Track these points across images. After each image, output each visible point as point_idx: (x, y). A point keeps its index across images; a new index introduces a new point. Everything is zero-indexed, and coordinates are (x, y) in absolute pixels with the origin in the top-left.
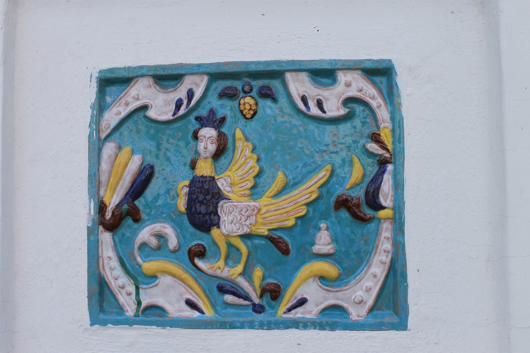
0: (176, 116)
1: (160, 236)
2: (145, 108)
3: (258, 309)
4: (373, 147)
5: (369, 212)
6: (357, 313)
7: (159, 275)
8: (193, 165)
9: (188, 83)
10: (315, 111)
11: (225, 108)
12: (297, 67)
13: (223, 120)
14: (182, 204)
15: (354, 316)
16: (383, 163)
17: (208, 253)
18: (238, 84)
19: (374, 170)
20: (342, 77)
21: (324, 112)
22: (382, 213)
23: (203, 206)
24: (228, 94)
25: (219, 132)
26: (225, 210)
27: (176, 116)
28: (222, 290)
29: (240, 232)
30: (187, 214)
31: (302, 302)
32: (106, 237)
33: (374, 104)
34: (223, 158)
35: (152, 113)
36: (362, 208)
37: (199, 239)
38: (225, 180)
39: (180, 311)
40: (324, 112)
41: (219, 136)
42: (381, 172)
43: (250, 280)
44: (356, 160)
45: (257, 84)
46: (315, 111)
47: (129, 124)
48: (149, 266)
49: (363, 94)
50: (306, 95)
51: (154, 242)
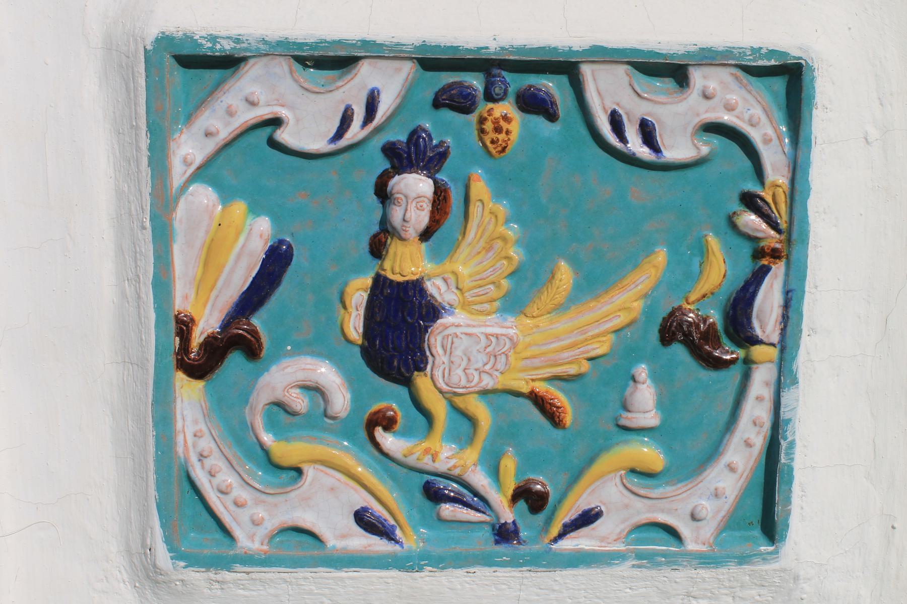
0: (343, 143)
1: (315, 390)
2: (276, 122)
3: (505, 534)
4: (750, 220)
5: (729, 351)
6: (695, 539)
7: (305, 467)
8: (377, 249)
9: (367, 75)
10: (636, 145)
11: (448, 129)
12: (604, 56)
13: (443, 156)
14: (355, 326)
15: (691, 546)
16: (763, 257)
17: (398, 427)
18: (476, 82)
19: (746, 267)
20: (697, 77)
21: (656, 149)
22: (757, 351)
23: (398, 330)
24: (455, 101)
25: (436, 182)
26: (145, 299)
27: (343, 143)
28: (433, 495)
29: (488, 382)
30: (362, 347)
31: (588, 518)
32: (189, 392)
33: (755, 136)
34: (207, 113)
35: (284, 136)
36: (719, 339)
37: (390, 398)
38: (445, 280)
39: (344, 537)
40: (656, 149)
41: (435, 193)
42: (758, 277)
43: (495, 472)
44: (714, 242)
45: (516, 82)
46: (636, 145)
47: (231, 151)
48: (287, 450)
49: (738, 117)
50: (621, 111)
51: (300, 402)
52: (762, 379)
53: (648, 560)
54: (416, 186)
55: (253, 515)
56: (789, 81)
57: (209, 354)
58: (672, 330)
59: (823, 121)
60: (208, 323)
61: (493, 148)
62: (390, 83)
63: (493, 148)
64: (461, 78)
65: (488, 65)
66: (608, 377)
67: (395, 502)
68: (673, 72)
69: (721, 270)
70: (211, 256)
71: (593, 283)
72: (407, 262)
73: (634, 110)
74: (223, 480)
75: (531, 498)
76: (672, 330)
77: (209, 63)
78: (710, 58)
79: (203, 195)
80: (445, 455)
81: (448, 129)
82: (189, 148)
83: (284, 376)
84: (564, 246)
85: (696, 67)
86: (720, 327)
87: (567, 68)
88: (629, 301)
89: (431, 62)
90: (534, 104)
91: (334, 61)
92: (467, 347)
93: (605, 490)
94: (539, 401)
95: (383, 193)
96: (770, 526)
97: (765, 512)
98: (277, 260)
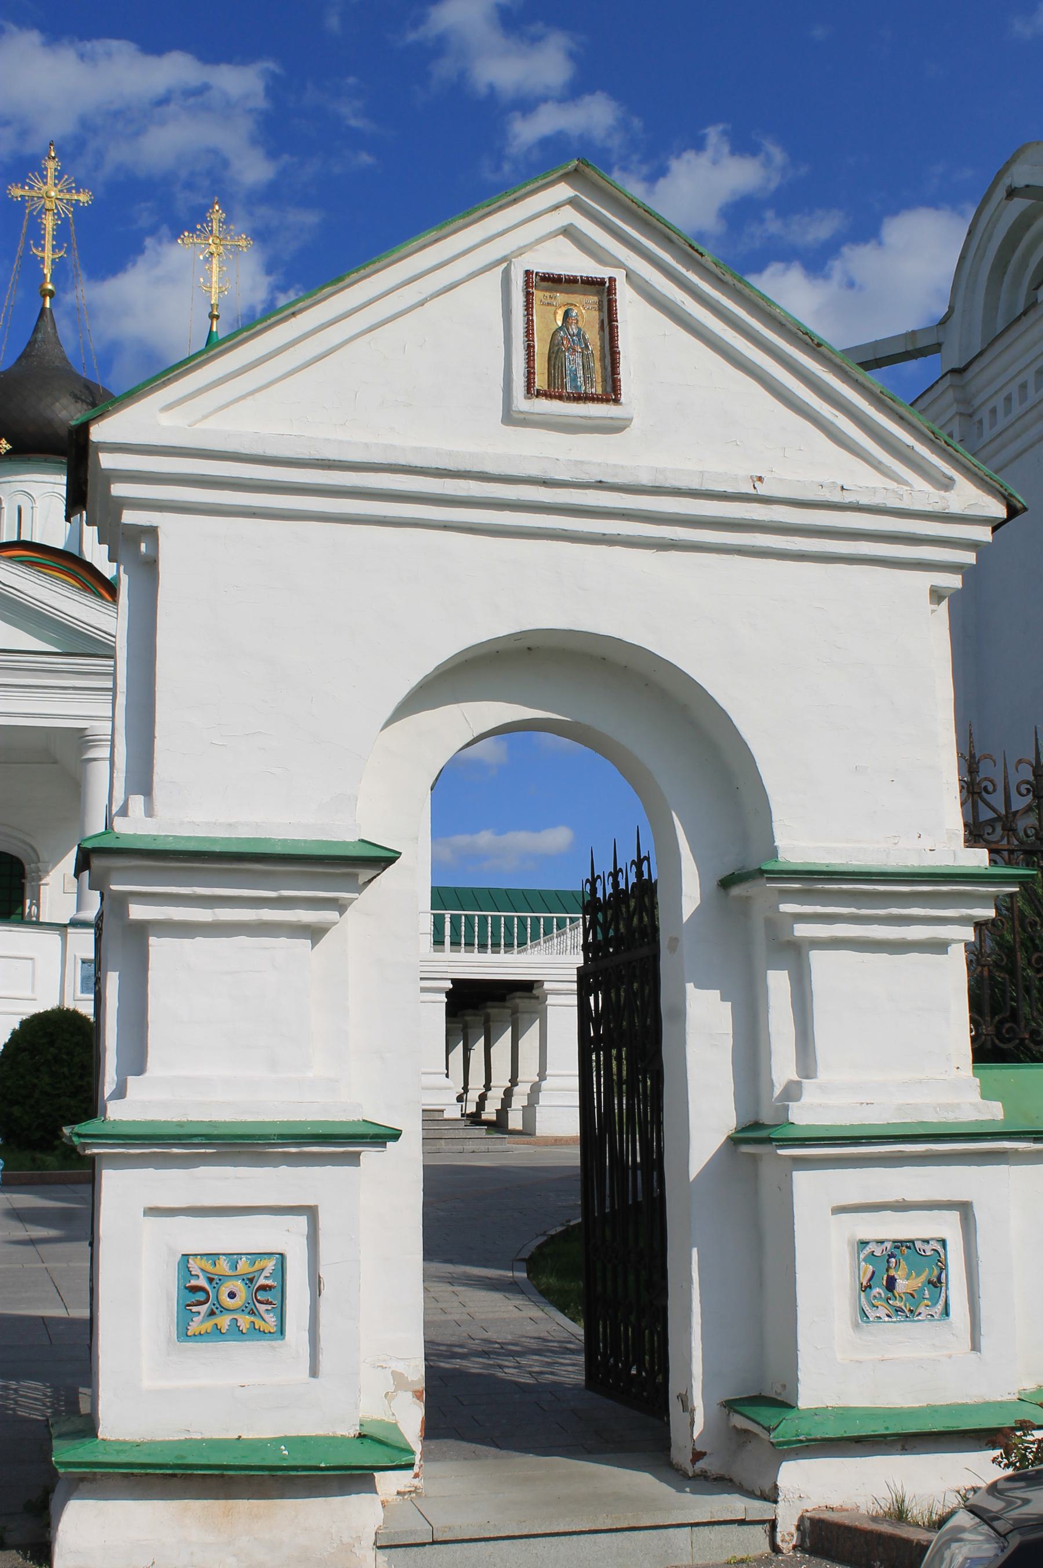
1: (879, 1294)
8: (887, 1271)
9: (886, 1244)
11: (896, 1252)
12: (918, 1240)
23: (891, 1284)
32: (863, 1294)
37: (890, 1295)
48: (875, 1302)
52: (943, 1289)
53: (930, 1320)
54: (893, 1260)
55: (872, 1314)
56: (943, 1242)
57: (866, 1288)
58: (930, 1282)
59: (948, 1248)
60: (864, 1284)
61: (902, 1254)
62: (888, 1245)
63: (902, 1254)
64: (899, 1244)
65: (901, 1242)
66: (921, 1290)
67: (892, 1312)
68: (927, 1241)
69: (936, 1272)
70: (865, 1273)
71: (918, 1275)
72: (892, 1273)
73: (922, 1247)
74: (867, 1309)
75: (911, 1311)
76: (930, 1282)
77: (864, 1243)
78: (932, 1239)
79: (863, 1263)
80: (898, 1303)
81: (896, 1252)
82: (862, 1256)
83: (876, 1291)
84: (914, 1269)
85: (237, 901)
86: (807, 1531)
87: (912, 1242)
88: (923, 1278)
89: (894, 1242)
90: (908, 1247)
91: (882, 1242)
92: (902, 1285)
93: (921, 1309)
94: (912, 1295)
95: (888, 1262)
96: (947, 1314)
97: (946, 1312)
98: (873, 1273)
